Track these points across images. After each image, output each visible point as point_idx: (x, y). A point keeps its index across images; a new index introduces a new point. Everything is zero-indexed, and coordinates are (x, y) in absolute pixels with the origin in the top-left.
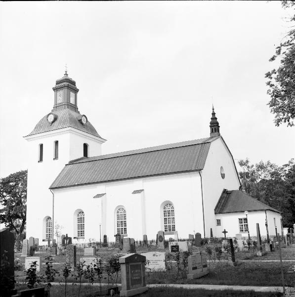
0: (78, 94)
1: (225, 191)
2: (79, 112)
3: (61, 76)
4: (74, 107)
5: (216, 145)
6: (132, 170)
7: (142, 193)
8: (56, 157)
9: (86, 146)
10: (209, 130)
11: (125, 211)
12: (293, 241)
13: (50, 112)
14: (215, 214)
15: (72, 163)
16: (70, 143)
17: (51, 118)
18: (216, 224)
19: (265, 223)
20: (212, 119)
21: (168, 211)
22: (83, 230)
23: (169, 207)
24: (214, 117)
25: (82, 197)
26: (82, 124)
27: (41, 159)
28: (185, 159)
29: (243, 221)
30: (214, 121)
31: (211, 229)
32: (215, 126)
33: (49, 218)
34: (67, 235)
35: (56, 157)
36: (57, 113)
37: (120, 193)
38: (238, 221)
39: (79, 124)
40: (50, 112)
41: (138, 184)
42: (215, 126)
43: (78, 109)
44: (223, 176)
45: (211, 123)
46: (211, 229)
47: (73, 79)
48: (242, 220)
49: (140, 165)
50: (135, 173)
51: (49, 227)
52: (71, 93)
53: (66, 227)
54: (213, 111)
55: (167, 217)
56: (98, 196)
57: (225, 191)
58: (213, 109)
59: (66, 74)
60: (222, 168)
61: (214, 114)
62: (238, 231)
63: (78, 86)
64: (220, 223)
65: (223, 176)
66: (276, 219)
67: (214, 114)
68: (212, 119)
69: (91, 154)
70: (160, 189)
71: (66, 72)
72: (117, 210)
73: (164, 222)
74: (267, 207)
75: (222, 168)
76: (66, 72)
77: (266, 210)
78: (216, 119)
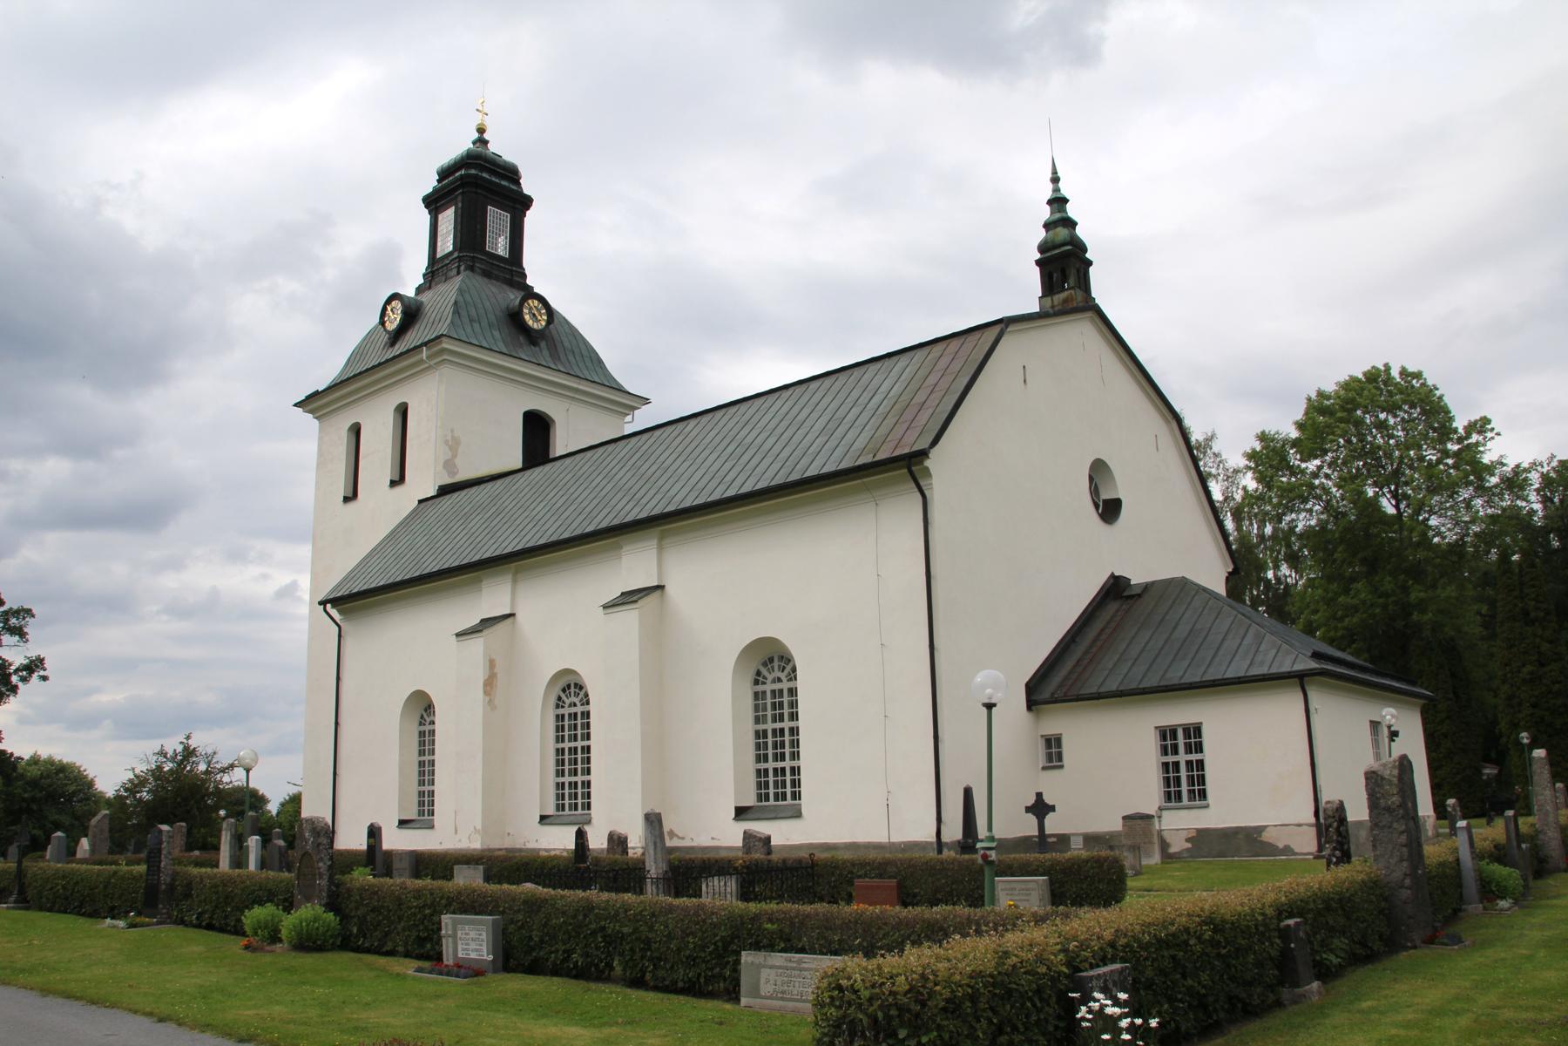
1: (1115, 588)
3: (462, 144)
4: (510, 270)
8: (398, 480)
12: (800, 961)
14: (1029, 708)
15: (445, 491)
18: (1042, 761)
19: (1291, 765)
20: (1047, 226)
23: (778, 674)
26: (532, 335)
30: (1062, 233)
35: (398, 480)
38: (1152, 744)
41: (635, 565)
42: (1064, 263)
43: (525, 276)
44: (1110, 510)
45: (1043, 248)
47: (508, 156)
48: (1174, 732)
51: (574, 751)
52: (452, 209)
54: (1056, 190)
57: (1115, 588)
58: (1055, 180)
61: (1058, 202)
62: (1146, 794)
64: (1060, 757)
65: (1110, 510)
67: (1058, 202)
68: (1047, 226)
71: (481, 131)
72: (557, 690)
73: (415, 778)
76: (481, 131)
77: (1300, 679)
78: (1070, 224)
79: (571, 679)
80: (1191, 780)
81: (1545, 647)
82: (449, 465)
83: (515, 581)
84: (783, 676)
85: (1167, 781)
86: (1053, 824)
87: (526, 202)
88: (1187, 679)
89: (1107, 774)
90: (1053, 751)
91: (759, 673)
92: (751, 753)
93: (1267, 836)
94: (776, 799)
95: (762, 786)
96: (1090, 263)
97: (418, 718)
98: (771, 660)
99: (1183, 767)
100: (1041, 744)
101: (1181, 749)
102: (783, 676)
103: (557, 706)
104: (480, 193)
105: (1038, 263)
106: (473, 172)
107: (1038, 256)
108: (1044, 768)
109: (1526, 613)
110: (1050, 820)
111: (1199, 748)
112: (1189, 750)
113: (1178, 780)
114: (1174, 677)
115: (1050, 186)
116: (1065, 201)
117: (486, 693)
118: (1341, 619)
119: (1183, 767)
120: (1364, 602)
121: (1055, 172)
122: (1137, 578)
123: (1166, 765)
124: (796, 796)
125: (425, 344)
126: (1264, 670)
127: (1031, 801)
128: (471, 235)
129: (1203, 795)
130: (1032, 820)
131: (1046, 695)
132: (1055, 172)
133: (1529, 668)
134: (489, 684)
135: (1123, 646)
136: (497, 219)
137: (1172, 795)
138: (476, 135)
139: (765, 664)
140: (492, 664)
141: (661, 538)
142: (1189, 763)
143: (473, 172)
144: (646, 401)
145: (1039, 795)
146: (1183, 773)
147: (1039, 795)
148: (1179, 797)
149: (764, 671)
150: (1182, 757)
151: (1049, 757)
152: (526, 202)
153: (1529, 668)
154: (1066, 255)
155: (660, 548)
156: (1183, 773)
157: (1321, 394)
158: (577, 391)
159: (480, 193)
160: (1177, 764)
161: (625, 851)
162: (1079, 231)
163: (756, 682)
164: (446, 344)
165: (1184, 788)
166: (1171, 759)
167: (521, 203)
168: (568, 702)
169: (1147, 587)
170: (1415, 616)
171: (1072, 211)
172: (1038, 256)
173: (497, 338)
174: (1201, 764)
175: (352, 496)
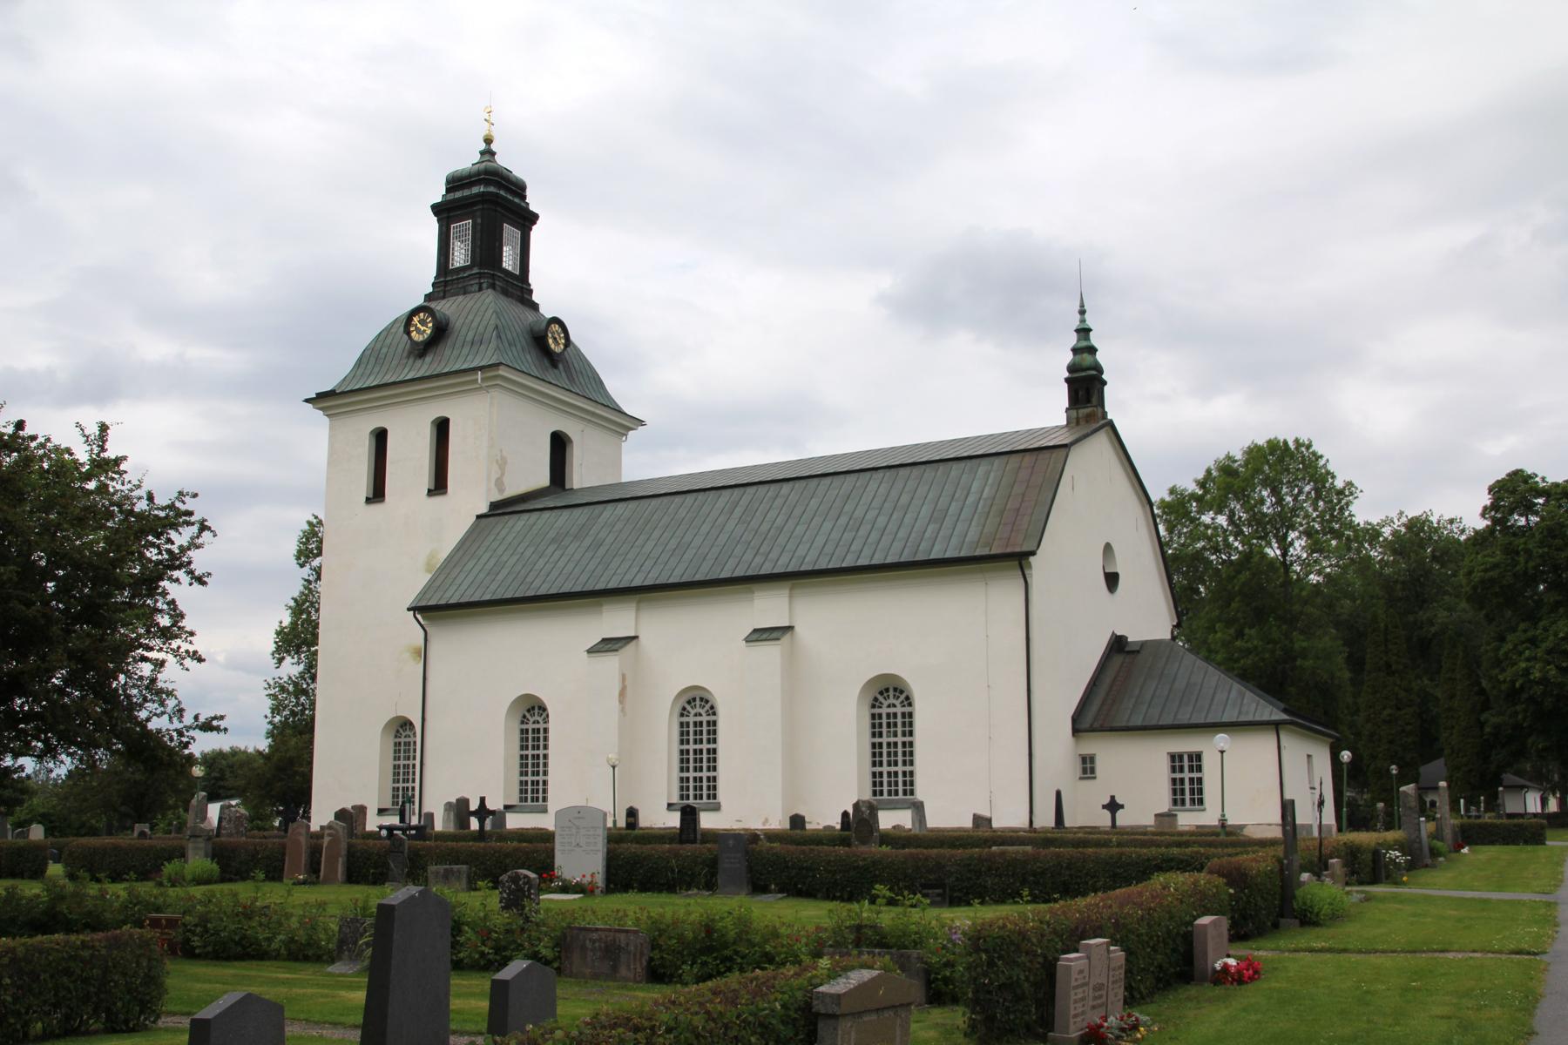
0: (536, 233)
1: (1118, 645)
3: (467, 160)
4: (518, 287)
5: (1090, 465)
7: (786, 638)
8: (439, 485)
9: (559, 444)
10: (1060, 397)
14: (1076, 731)
15: (500, 509)
16: (499, 439)
17: (423, 331)
18: (1079, 773)
19: (1263, 781)
21: (889, 708)
24: (1084, 344)
25: (546, 656)
26: (549, 353)
27: (377, 493)
28: (961, 518)
29: (1186, 763)
30: (1087, 358)
31: (1058, 794)
32: (1086, 386)
33: (404, 725)
35: (439, 485)
36: (444, 307)
37: (694, 646)
38: (1164, 765)
39: (530, 360)
40: (420, 301)
42: (1086, 386)
43: (531, 292)
44: (1112, 580)
46: (1058, 794)
47: (518, 172)
50: (759, 559)
53: (468, 770)
54: (1083, 321)
55: (885, 769)
56: (609, 645)
57: (1118, 645)
58: (1082, 312)
59: (488, 153)
60: (1108, 548)
61: (1084, 332)
63: (534, 202)
64: (1093, 770)
65: (1112, 580)
66: (1315, 760)
68: (1075, 351)
69: (583, 474)
70: (858, 635)
71: (488, 141)
74: (1271, 712)
75: (1108, 548)
76: (488, 141)
77: (1276, 726)
78: (1092, 350)
79: (698, 694)
80: (1192, 791)
81: (1402, 694)
82: (499, 484)
83: (638, 610)
84: (897, 703)
85: (1174, 792)
86: (1123, 819)
87: (532, 218)
88: (1194, 721)
89: (1134, 783)
90: (1088, 767)
91: (876, 699)
92: (868, 759)
93: (1246, 832)
94: (890, 793)
95: (523, 791)
96: (1105, 383)
97: (520, 718)
98: (887, 690)
99: (1187, 782)
100: (1079, 761)
101: (1186, 769)
102: (897, 703)
104: (486, 208)
105: (1067, 380)
106: (492, 189)
107: (1067, 375)
109: (1388, 666)
110: (1119, 813)
111: (1199, 769)
112: (1191, 769)
113: (1183, 791)
114: (1184, 718)
115: (1078, 317)
116: (1089, 330)
117: (621, 702)
118: (1237, 661)
119: (1187, 782)
120: (1256, 648)
121: (1082, 305)
124: (545, 799)
125: (481, 368)
126: (1250, 718)
127: (1107, 801)
128: (486, 252)
129: (1201, 802)
130: (1107, 814)
131: (1086, 725)
132: (1082, 305)
133: (1388, 711)
134: (622, 693)
135: (1137, 692)
136: (510, 232)
137: (1178, 801)
138: (483, 146)
139: (881, 693)
140: (624, 677)
141: (791, 589)
142: (1192, 780)
143: (492, 189)
144: (641, 422)
145: (1113, 798)
146: (1187, 786)
147: (1113, 798)
148: (1183, 803)
149: (881, 698)
150: (1187, 775)
151: (1084, 771)
152: (532, 218)
153: (1388, 711)
155: (791, 597)
156: (1187, 786)
157: (1229, 457)
158: (594, 414)
159: (486, 208)
160: (1182, 780)
161: (803, 827)
162: (1099, 357)
163: (873, 706)
164: (502, 372)
165: (1187, 796)
167: (527, 220)
170: (1299, 662)
171: (1094, 340)
172: (1067, 375)
174: (1200, 780)
175: (377, 493)
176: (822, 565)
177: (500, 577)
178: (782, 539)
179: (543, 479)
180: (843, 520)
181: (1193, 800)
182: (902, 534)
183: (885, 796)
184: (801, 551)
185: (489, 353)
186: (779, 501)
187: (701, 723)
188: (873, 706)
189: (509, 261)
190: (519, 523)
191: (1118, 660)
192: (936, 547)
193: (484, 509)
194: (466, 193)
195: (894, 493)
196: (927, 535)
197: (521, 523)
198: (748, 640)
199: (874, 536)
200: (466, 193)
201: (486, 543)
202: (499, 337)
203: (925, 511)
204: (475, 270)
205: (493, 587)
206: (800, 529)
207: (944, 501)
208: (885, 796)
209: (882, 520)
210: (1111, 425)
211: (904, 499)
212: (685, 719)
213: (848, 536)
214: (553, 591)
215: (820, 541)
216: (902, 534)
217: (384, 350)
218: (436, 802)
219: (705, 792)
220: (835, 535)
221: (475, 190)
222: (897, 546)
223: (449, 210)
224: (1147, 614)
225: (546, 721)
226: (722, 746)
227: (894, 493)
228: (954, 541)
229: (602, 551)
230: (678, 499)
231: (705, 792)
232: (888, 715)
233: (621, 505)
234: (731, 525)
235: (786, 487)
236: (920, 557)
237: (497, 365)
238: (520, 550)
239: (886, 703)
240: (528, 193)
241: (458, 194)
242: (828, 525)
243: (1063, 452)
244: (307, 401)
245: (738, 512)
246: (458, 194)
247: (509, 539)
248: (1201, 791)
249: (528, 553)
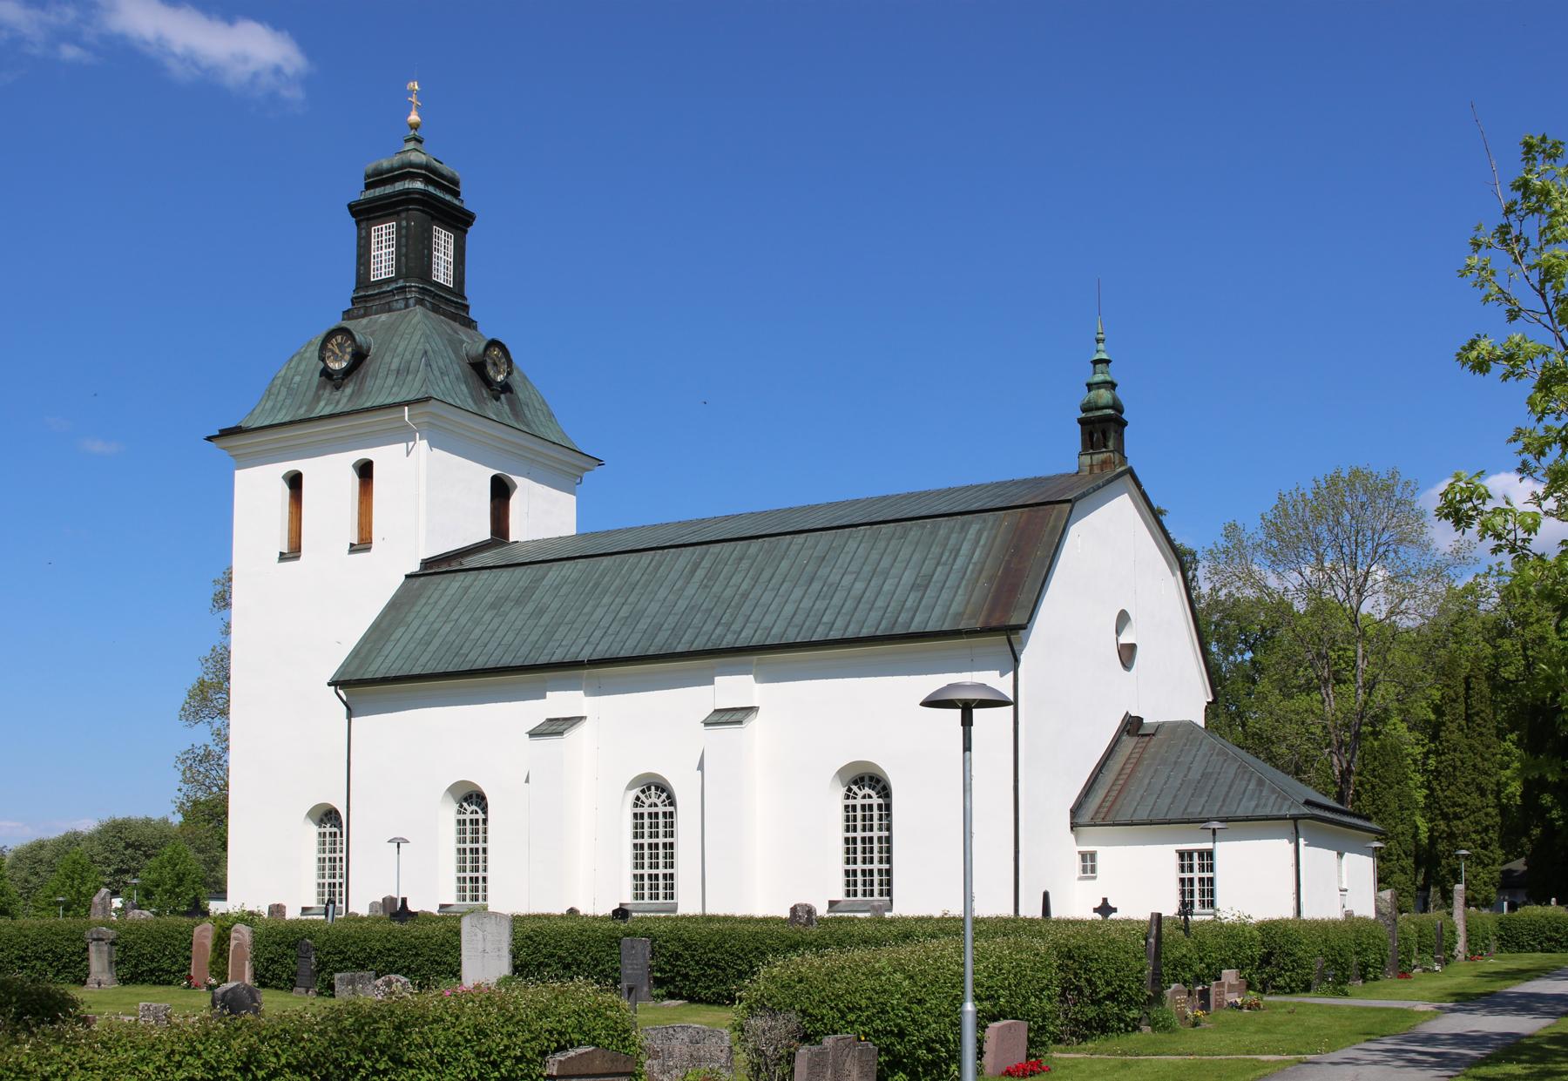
1: (1132, 725)
2: (470, 324)
4: (451, 304)
6: (605, 592)
8: (363, 544)
9: (501, 491)
11: (671, 800)
13: (333, 326)
14: (1073, 826)
15: (435, 566)
21: (654, 806)
22: (480, 846)
30: (1104, 396)
31: (1046, 896)
32: (1102, 429)
34: (404, 901)
35: (363, 544)
38: (1175, 860)
41: (733, 688)
42: (1102, 429)
44: (1127, 654)
46: (1046, 896)
49: (745, 596)
57: (1132, 725)
65: (1127, 654)
72: (636, 791)
80: (1202, 892)
89: (1138, 881)
95: (638, 888)
102: (659, 802)
103: (636, 805)
108: (1081, 879)
111: (1211, 868)
122: (1149, 719)
123: (1182, 880)
125: (408, 403)
126: (1267, 811)
136: (443, 244)
145: (1105, 900)
147: (1105, 900)
149: (642, 797)
151: (1084, 870)
154: (1107, 419)
166: (1187, 875)
168: (647, 802)
169: (1159, 727)
173: (462, 393)
175: (293, 552)
176: (791, 637)
177: (432, 648)
178: (746, 609)
179: (486, 535)
180: (816, 586)
181: (1202, 903)
182: (880, 603)
183: (860, 897)
184: (767, 622)
185: (417, 384)
186: (745, 564)
187: (657, 814)
188: (848, 797)
189: (442, 272)
190: (456, 584)
191: (1129, 743)
192: (917, 619)
193: (416, 568)
194: (388, 189)
195: (874, 556)
196: (908, 604)
197: (456, 585)
198: (923, 704)
199: (849, 604)
200: (388, 189)
201: (417, 609)
202: (428, 365)
203: (908, 577)
204: (401, 283)
205: (423, 660)
206: (768, 596)
207: (929, 565)
208: (860, 897)
209: (859, 586)
210: (1131, 472)
211: (885, 563)
212: (639, 810)
213: (820, 605)
214: (490, 665)
215: (789, 609)
216: (880, 603)
217: (297, 379)
218: (361, 901)
219: (860, 888)
220: (806, 604)
221: (399, 186)
222: (839, 623)
223: (369, 211)
224: (1176, 690)
225: (485, 811)
226: (838, 834)
227: (874, 556)
228: (938, 611)
229: (545, 619)
230: (633, 558)
231: (860, 888)
232: (863, 807)
233: (568, 564)
234: (690, 591)
235: (755, 546)
236: (898, 630)
237: (428, 399)
238: (454, 616)
239: (860, 793)
240: (462, 189)
241: (378, 191)
242: (797, 593)
243: (1067, 506)
244: (209, 439)
245: (700, 573)
246: (378, 191)
247: (442, 603)
248: (1212, 893)
249: (463, 620)
